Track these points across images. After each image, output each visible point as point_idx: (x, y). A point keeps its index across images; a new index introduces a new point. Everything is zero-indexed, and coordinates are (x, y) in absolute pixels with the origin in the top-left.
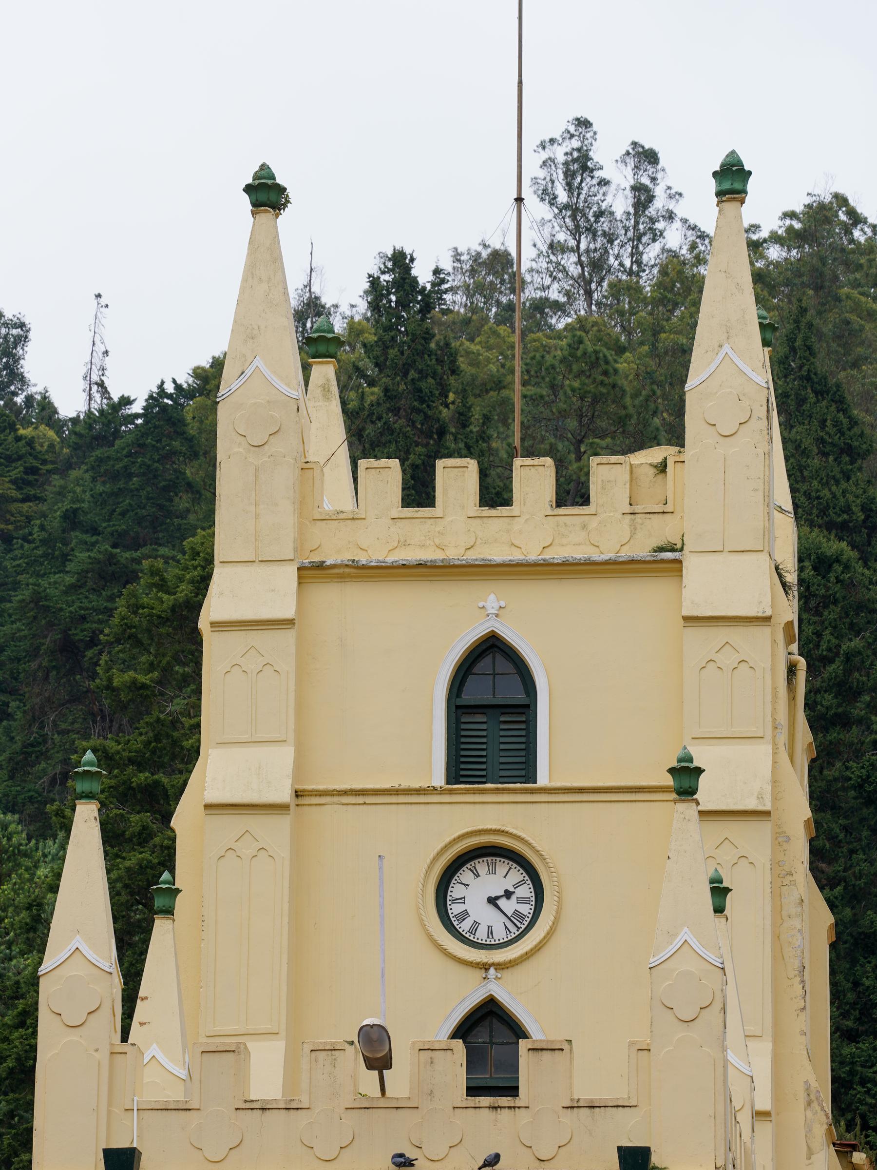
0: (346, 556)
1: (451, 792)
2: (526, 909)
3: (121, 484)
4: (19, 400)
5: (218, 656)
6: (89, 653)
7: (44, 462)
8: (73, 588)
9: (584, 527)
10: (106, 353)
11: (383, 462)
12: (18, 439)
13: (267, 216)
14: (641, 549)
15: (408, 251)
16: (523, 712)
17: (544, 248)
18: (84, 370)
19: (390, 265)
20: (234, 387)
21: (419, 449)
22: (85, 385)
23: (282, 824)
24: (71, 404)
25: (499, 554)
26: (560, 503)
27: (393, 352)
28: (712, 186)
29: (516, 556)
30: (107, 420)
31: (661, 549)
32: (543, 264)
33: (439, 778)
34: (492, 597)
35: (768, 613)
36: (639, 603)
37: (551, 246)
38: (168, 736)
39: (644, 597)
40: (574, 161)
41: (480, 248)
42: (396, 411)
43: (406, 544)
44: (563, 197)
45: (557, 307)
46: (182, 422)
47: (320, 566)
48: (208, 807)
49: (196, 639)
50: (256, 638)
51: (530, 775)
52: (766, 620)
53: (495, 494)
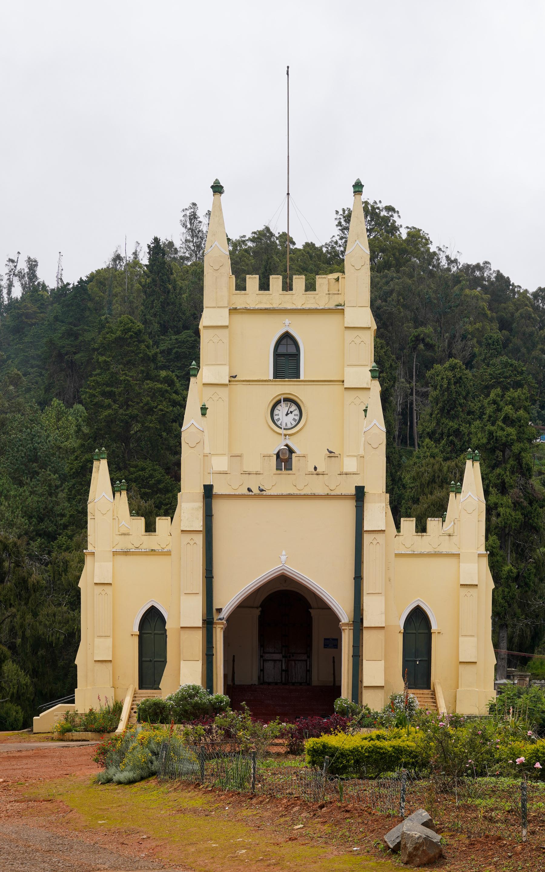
0: (243, 306)
1: (275, 381)
2: (297, 418)
3: (70, 308)
4: (36, 283)
5: (205, 337)
6: (66, 357)
7: (46, 302)
8: (61, 338)
9: (314, 298)
10: (62, 270)
11: (254, 276)
12: (39, 295)
13: (217, 196)
14: (332, 306)
15: (158, 237)
16: (296, 356)
17: (184, 241)
18: (56, 275)
19: (153, 241)
20: (209, 250)
21: (163, 297)
22: (56, 279)
23: (225, 390)
24: (52, 284)
25: (289, 306)
26: (306, 290)
27: (155, 268)
28: (352, 189)
29: (294, 307)
30: (64, 289)
31: (338, 306)
32: (184, 246)
33: (271, 377)
34: (287, 320)
35: (370, 326)
36: (330, 323)
37: (186, 240)
38: (115, 377)
39: (332, 320)
40: (192, 215)
41: (165, 241)
42: (156, 285)
43: (260, 303)
44: (189, 226)
45: (188, 259)
46: (87, 289)
47: (235, 309)
48: (204, 384)
49: (197, 333)
50: (217, 331)
51: (298, 377)
52: (369, 328)
53: (287, 287)
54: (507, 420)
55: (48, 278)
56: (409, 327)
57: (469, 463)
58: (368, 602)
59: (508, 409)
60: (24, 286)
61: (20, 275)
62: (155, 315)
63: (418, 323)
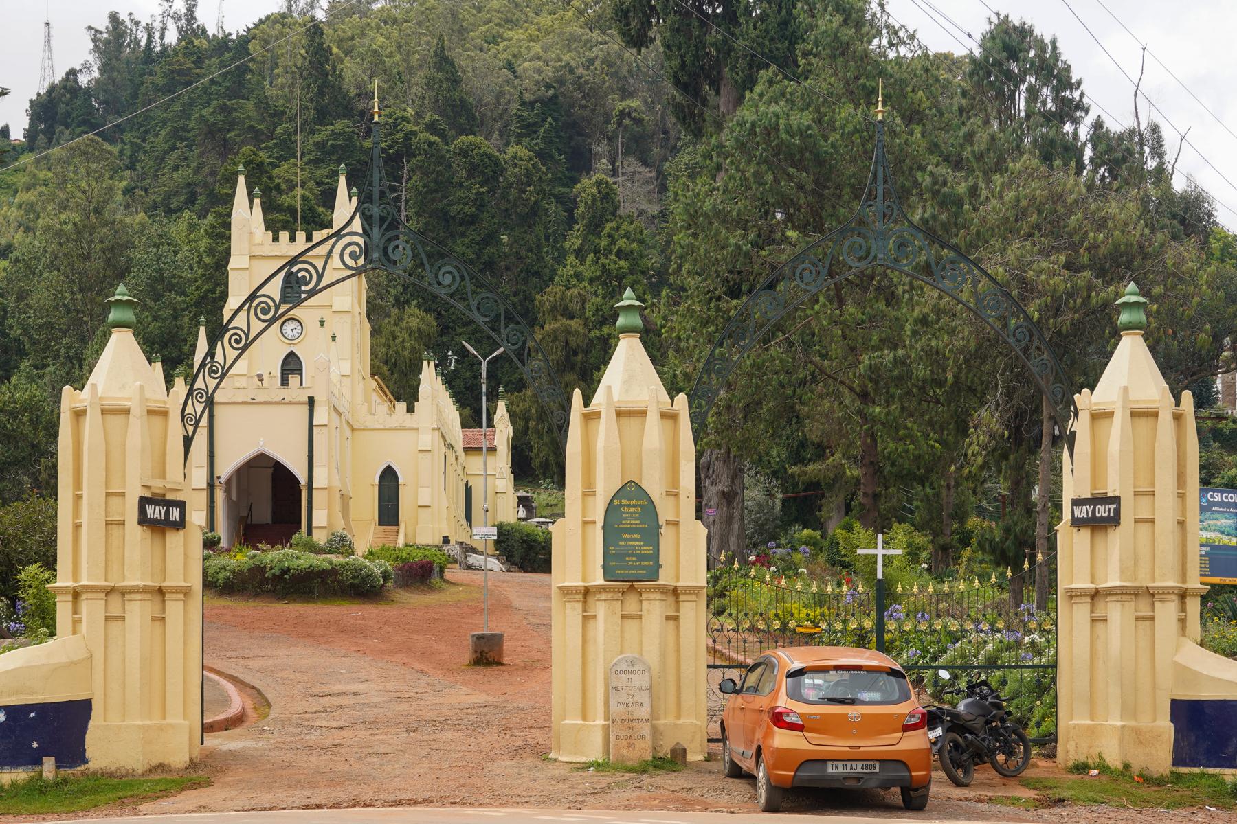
53: (293, 239)
54: (619, 254)
55: (209, 19)
56: (613, 100)
57: (425, 363)
58: (317, 471)
59: (622, 243)
60: (180, 30)
61: (176, 17)
62: (311, 101)
63: (626, 93)
